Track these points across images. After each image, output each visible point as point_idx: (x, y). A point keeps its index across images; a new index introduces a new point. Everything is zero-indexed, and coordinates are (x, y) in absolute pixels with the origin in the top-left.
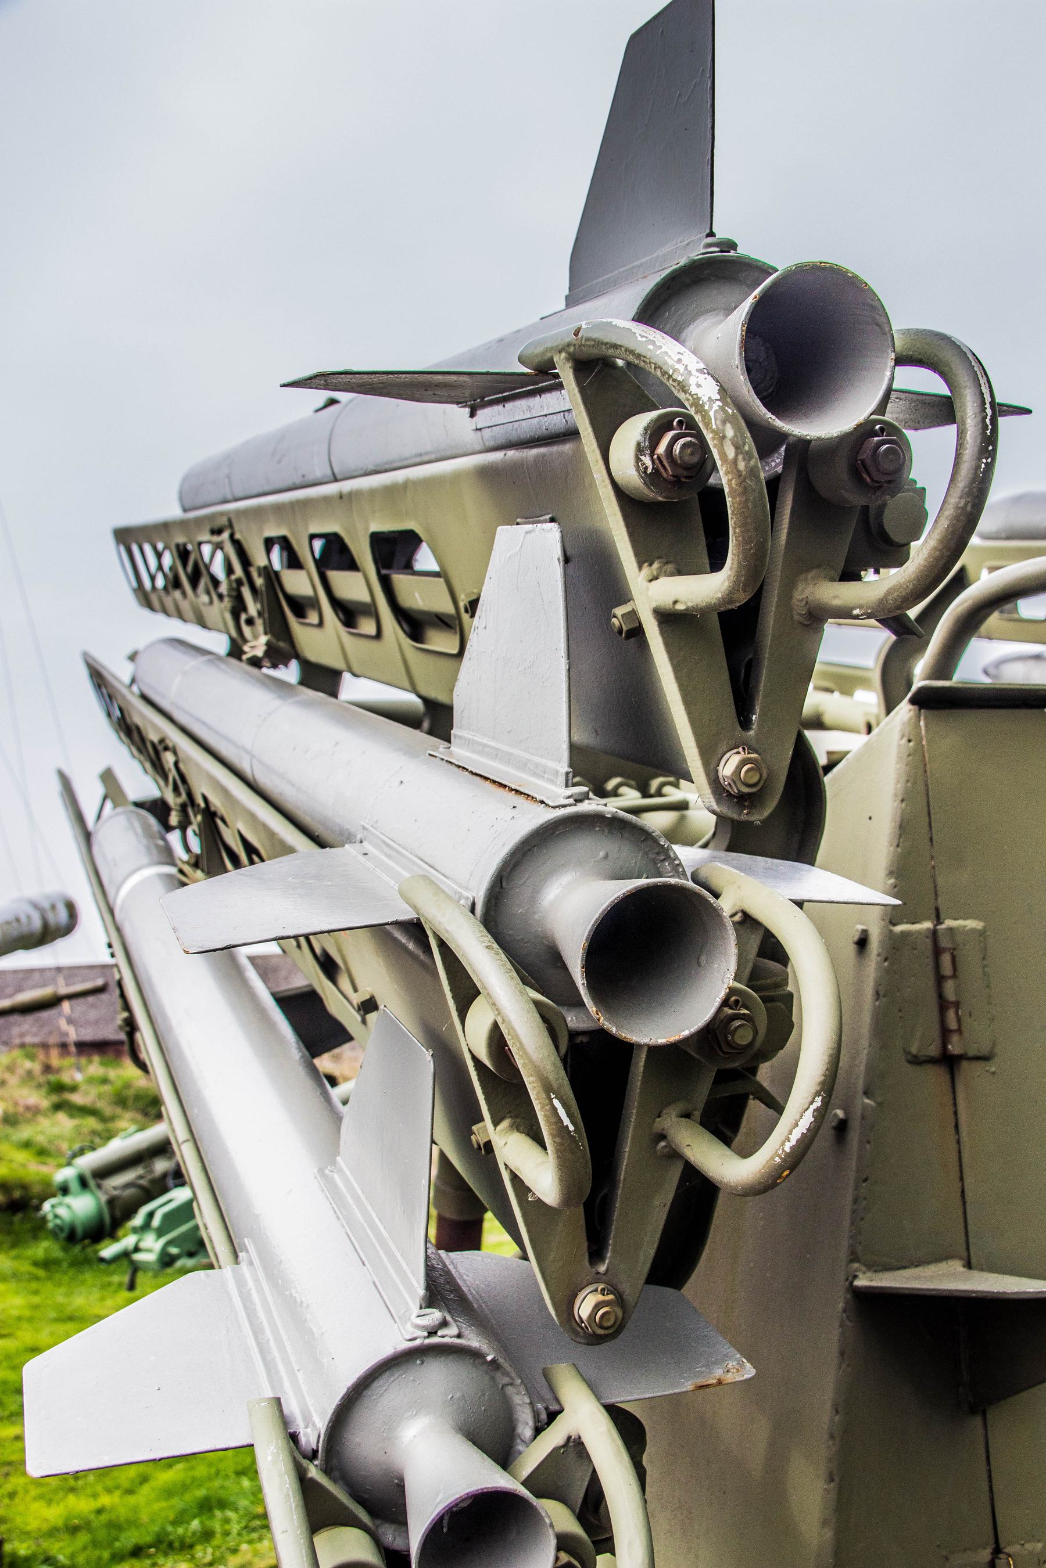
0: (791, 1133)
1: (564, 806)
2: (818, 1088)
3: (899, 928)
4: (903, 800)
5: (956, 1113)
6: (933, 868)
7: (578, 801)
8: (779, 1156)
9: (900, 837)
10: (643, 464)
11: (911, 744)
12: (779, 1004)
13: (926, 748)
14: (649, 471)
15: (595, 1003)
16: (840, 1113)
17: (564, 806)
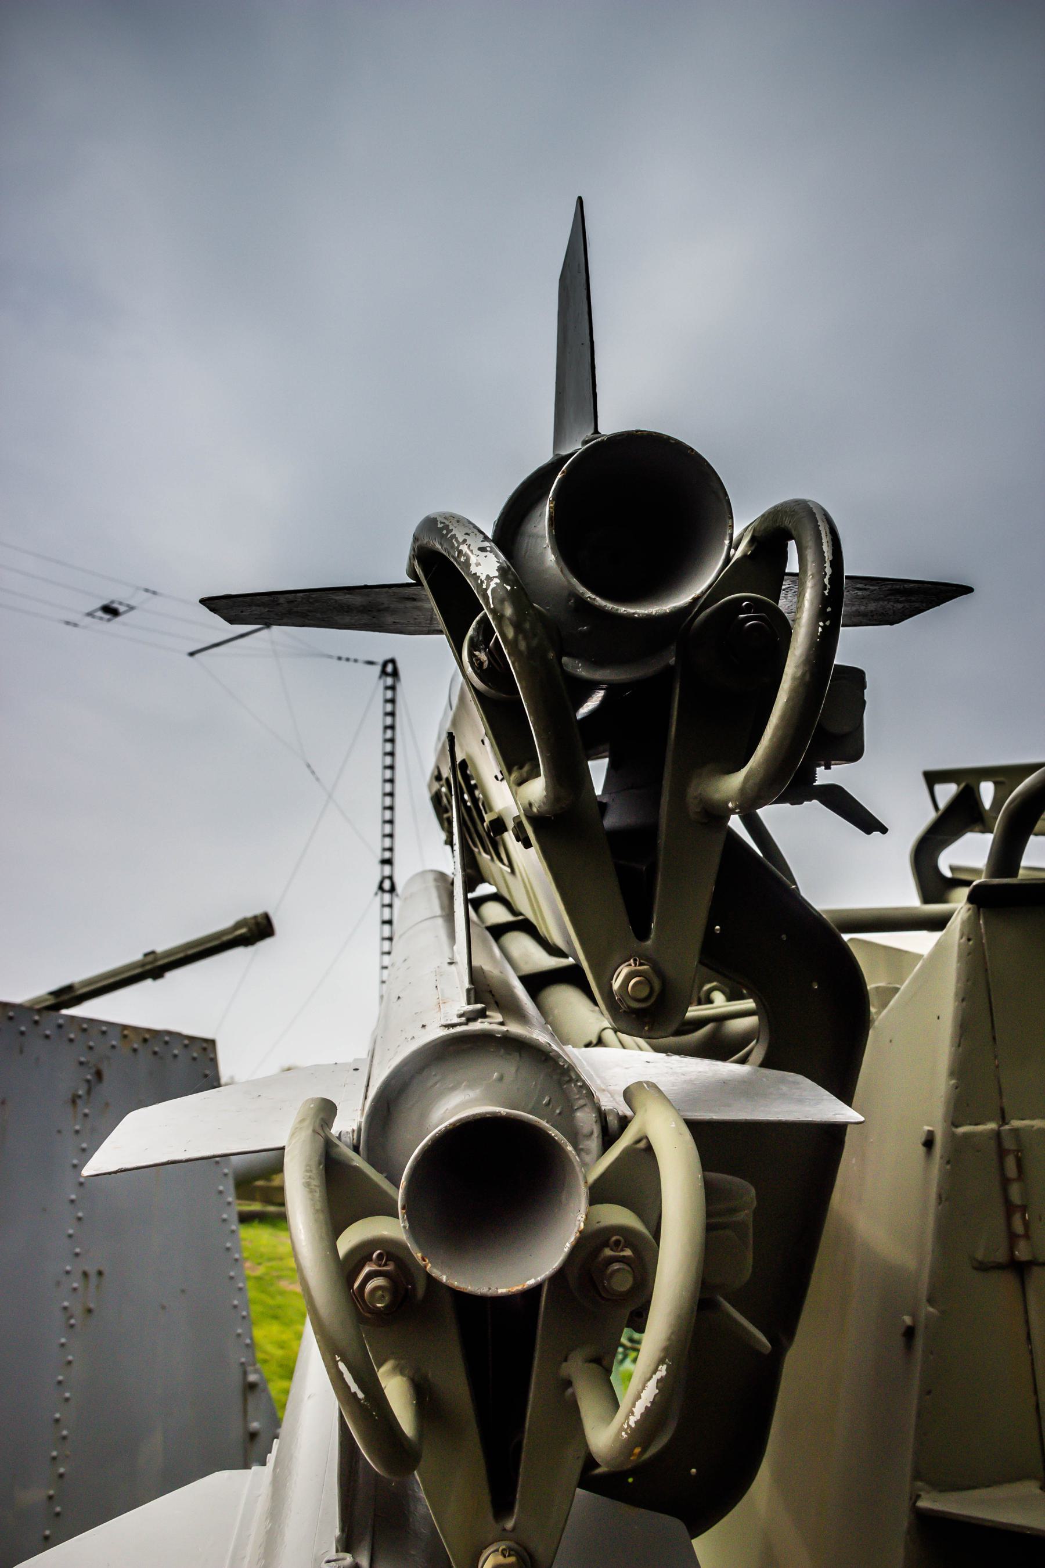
0: (634, 1405)
1: (453, 1026)
2: (662, 1355)
3: (961, 1130)
4: (963, 1000)
5: (1027, 1322)
6: (997, 1067)
7: (470, 1020)
8: (625, 1430)
9: (961, 1036)
10: (478, 659)
11: (971, 943)
12: (729, 1232)
13: (986, 947)
14: (486, 665)
15: (421, 1248)
16: (908, 1320)
17: (453, 1026)
